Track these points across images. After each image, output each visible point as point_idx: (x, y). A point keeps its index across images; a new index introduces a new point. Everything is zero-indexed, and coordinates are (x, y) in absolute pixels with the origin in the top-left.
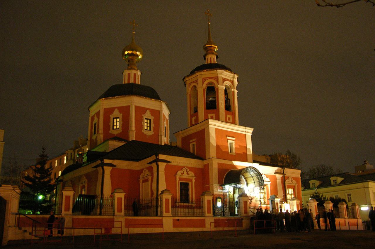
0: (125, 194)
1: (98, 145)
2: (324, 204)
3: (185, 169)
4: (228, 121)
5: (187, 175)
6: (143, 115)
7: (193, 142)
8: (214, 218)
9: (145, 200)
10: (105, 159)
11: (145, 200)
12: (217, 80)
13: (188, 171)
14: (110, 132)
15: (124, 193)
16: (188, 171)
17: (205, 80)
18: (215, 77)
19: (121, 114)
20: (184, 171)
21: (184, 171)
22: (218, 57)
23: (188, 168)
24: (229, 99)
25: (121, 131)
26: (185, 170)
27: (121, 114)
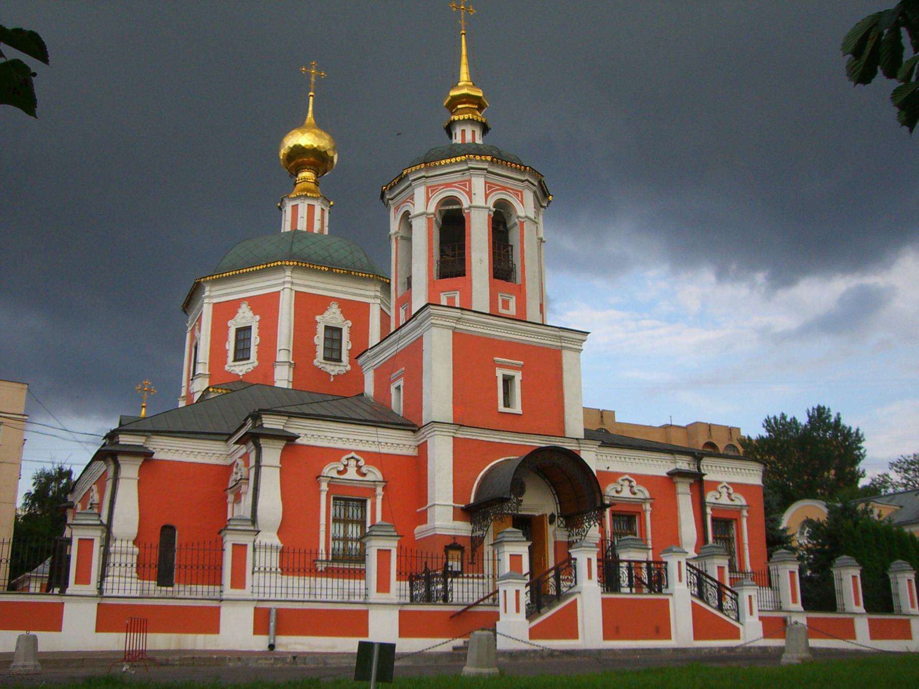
0: (529, 543)
1: (424, 424)
2: (832, 569)
3: (352, 458)
4: (502, 311)
5: (361, 478)
6: (318, 318)
7: (399, 378)
8: (98, 600)
9: (297, 550)
10: (415, 457)
11: (297, 550)
12: (467, 190)
13: (362, 463)
14: (227, 368)
15: (727, 555)
16: (362, 463)
17: (432, 191)
18: (461, 182)
19: (258, 318)
20: (346, 466)
21: (346, 466)
22: (489, 126)
23: (631, 477)
24: (512, 246)
25: (256, 363)
26: (353, 460)
27: (258, 318)
